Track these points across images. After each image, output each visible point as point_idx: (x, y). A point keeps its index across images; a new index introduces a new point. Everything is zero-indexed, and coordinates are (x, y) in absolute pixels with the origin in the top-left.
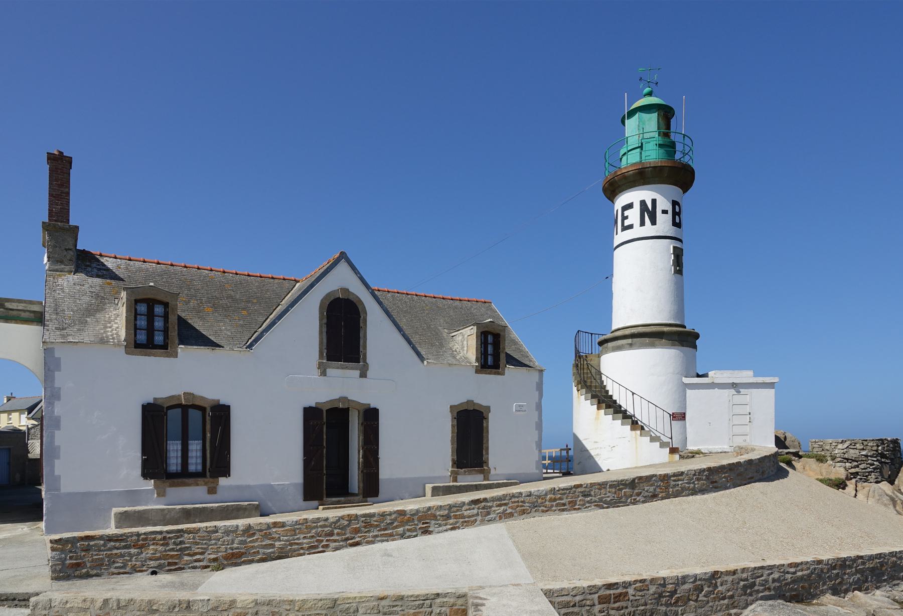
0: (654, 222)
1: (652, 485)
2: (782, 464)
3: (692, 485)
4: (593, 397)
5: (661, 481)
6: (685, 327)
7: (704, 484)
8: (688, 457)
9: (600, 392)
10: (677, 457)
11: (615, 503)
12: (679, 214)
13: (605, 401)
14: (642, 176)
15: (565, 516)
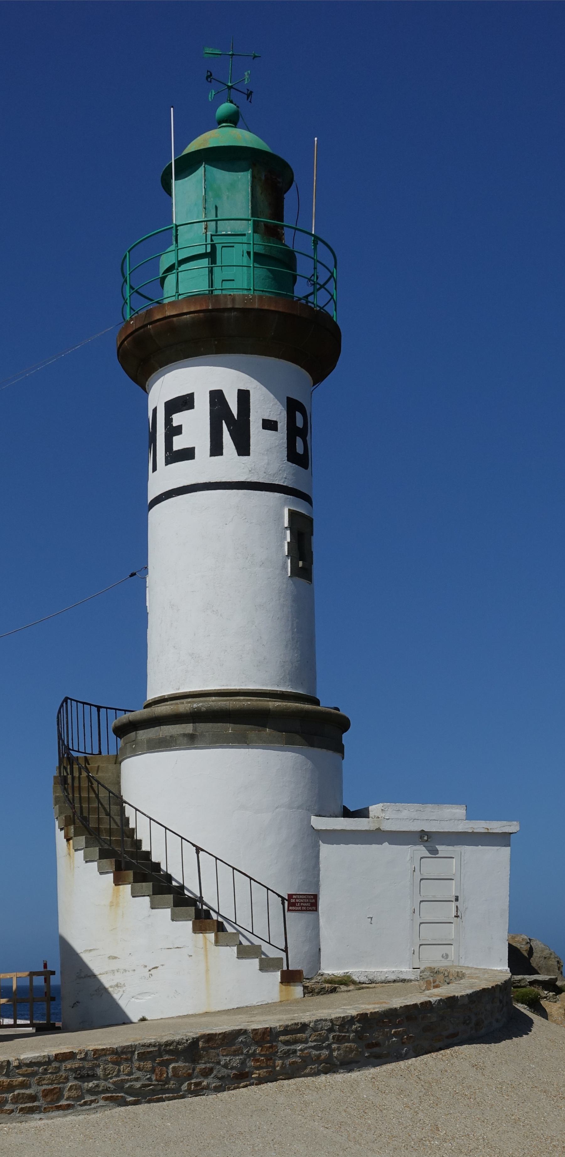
0: (243, 448)
1: (236, 1053)
2: (521, 1007)
3: (325, 1052)
4: (103, 855)
5: (258, 1043)
6: (317, 702)
7: (351, 1050)
8: (322, 992)
9: (121, 843)
10: (297, 991)
11: (154, 1092)
12: (303, 433)
13: (133, 865)
14: (211, 331)
15: (37, 1123)
